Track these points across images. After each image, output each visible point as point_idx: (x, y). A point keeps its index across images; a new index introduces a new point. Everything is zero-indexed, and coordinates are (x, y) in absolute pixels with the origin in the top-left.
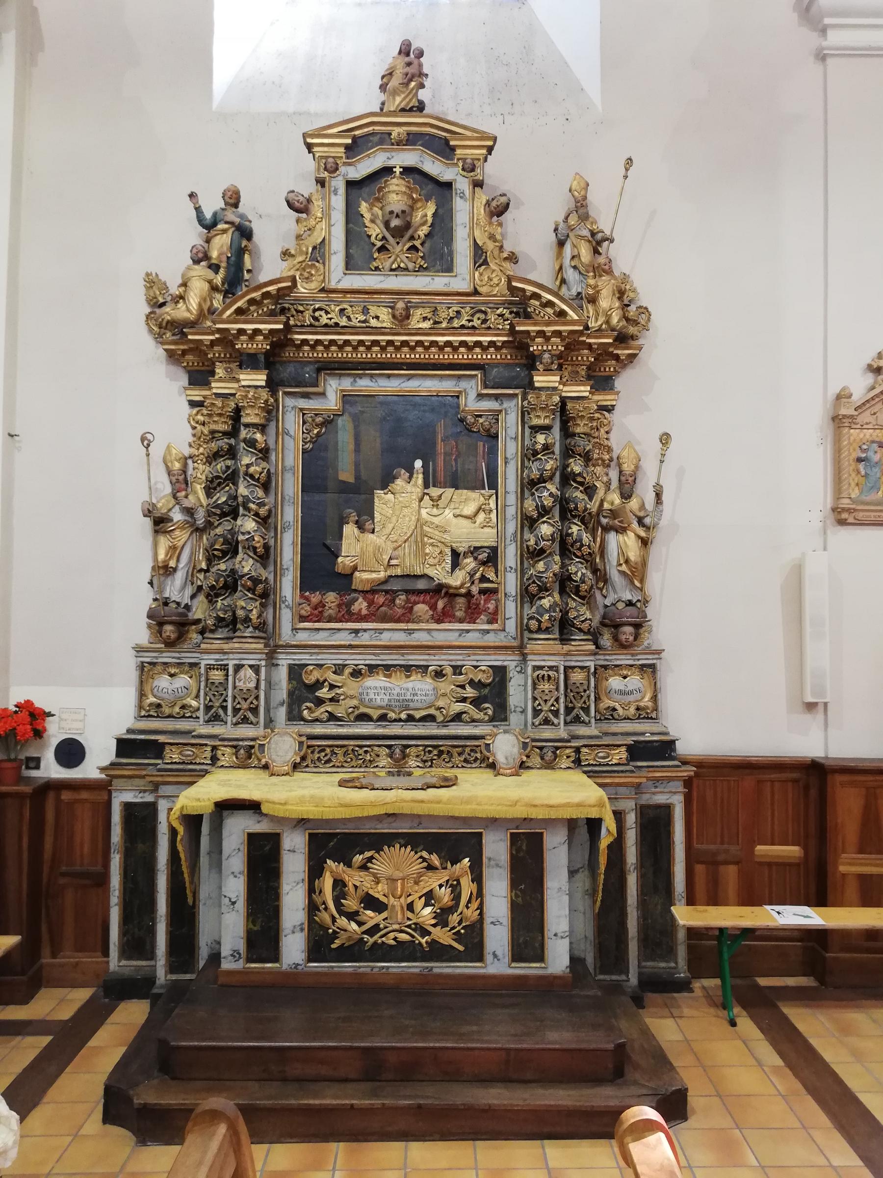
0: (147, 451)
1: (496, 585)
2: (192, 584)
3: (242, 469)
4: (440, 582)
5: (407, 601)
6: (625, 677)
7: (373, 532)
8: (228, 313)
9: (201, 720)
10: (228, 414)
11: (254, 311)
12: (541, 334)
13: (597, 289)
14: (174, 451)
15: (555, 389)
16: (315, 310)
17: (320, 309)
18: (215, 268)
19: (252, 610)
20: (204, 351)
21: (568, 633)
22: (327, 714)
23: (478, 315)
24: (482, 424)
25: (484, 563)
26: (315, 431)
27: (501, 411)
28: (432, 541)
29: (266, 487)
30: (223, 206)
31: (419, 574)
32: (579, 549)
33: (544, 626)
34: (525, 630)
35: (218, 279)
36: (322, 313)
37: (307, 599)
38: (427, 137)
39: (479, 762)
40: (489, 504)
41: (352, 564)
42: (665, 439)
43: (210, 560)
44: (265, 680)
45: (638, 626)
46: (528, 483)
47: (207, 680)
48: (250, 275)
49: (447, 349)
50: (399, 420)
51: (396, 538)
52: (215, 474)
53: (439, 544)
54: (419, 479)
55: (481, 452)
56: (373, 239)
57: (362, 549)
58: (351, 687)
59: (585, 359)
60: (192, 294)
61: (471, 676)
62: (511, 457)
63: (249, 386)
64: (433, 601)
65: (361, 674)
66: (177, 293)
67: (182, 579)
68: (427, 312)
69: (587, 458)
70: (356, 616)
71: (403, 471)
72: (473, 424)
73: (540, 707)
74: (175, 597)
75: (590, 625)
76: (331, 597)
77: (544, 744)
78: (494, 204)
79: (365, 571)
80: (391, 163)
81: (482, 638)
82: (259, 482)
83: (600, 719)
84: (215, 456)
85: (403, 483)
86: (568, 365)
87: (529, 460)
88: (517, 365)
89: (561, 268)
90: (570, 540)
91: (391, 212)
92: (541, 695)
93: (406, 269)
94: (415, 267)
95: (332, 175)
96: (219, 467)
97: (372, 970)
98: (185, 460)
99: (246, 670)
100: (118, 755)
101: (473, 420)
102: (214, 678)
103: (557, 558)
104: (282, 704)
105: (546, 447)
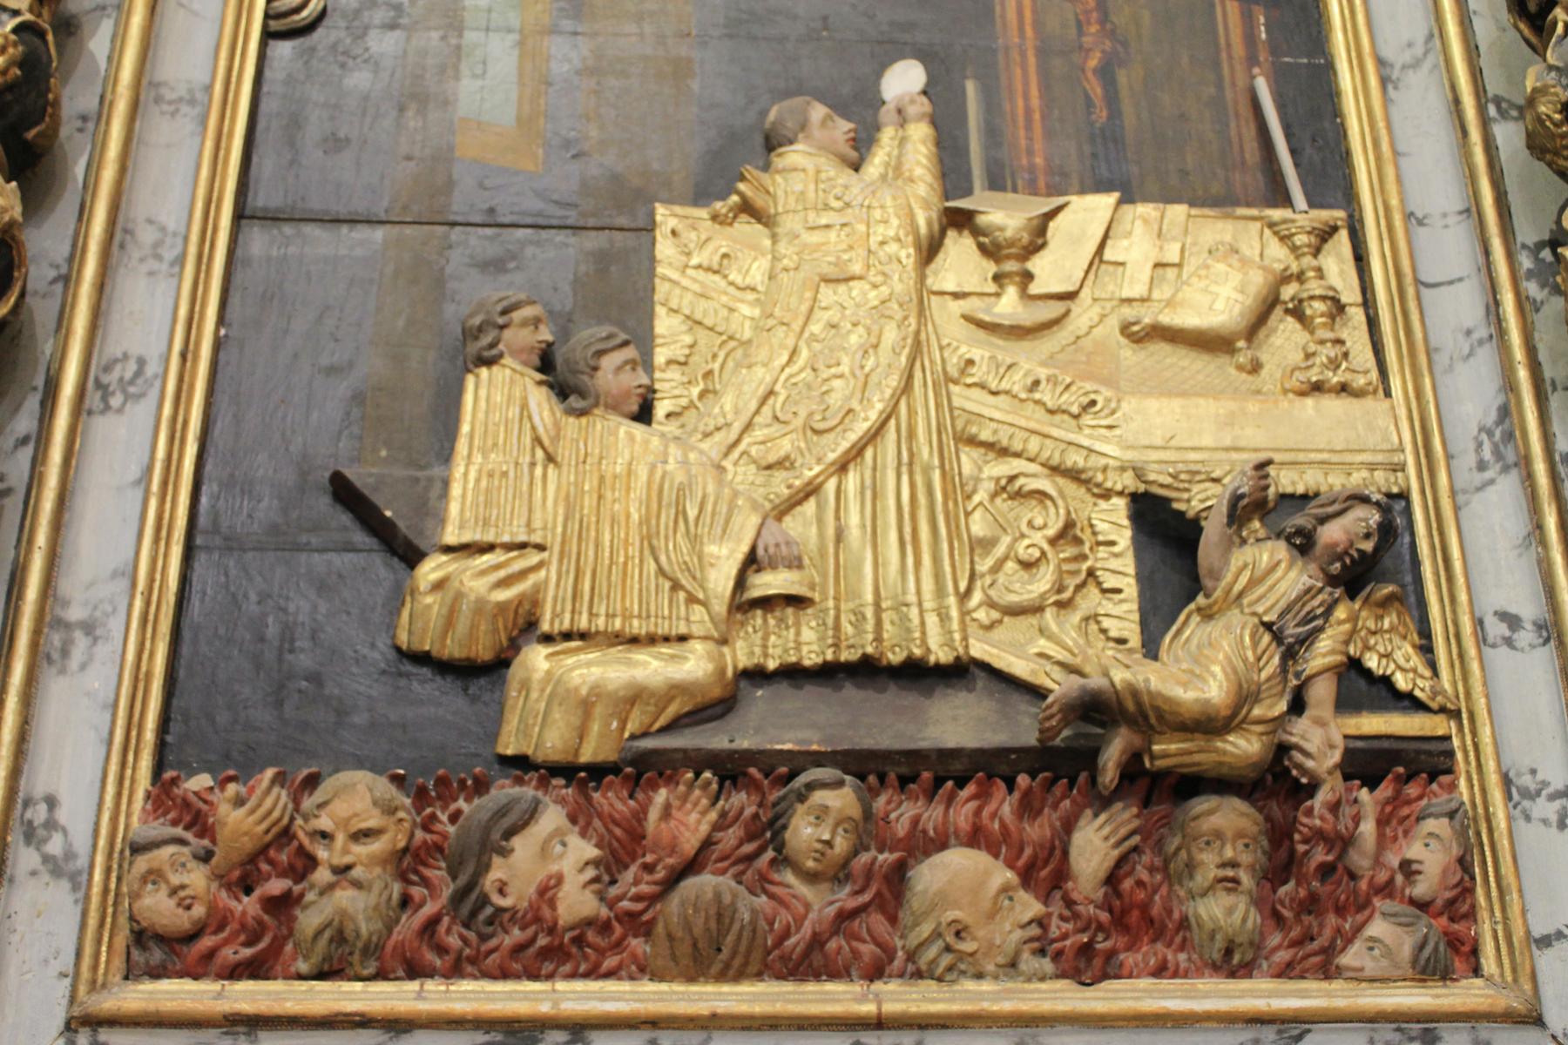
4: (1096, 682)
5: (868, 829)
7: (644, 414)
31: (941, 655)
37: (197, 819)
57: (570, 506)
62: (1407, 57)
64: (1037, 831)
70: (516, 936)
71: (818, 111)
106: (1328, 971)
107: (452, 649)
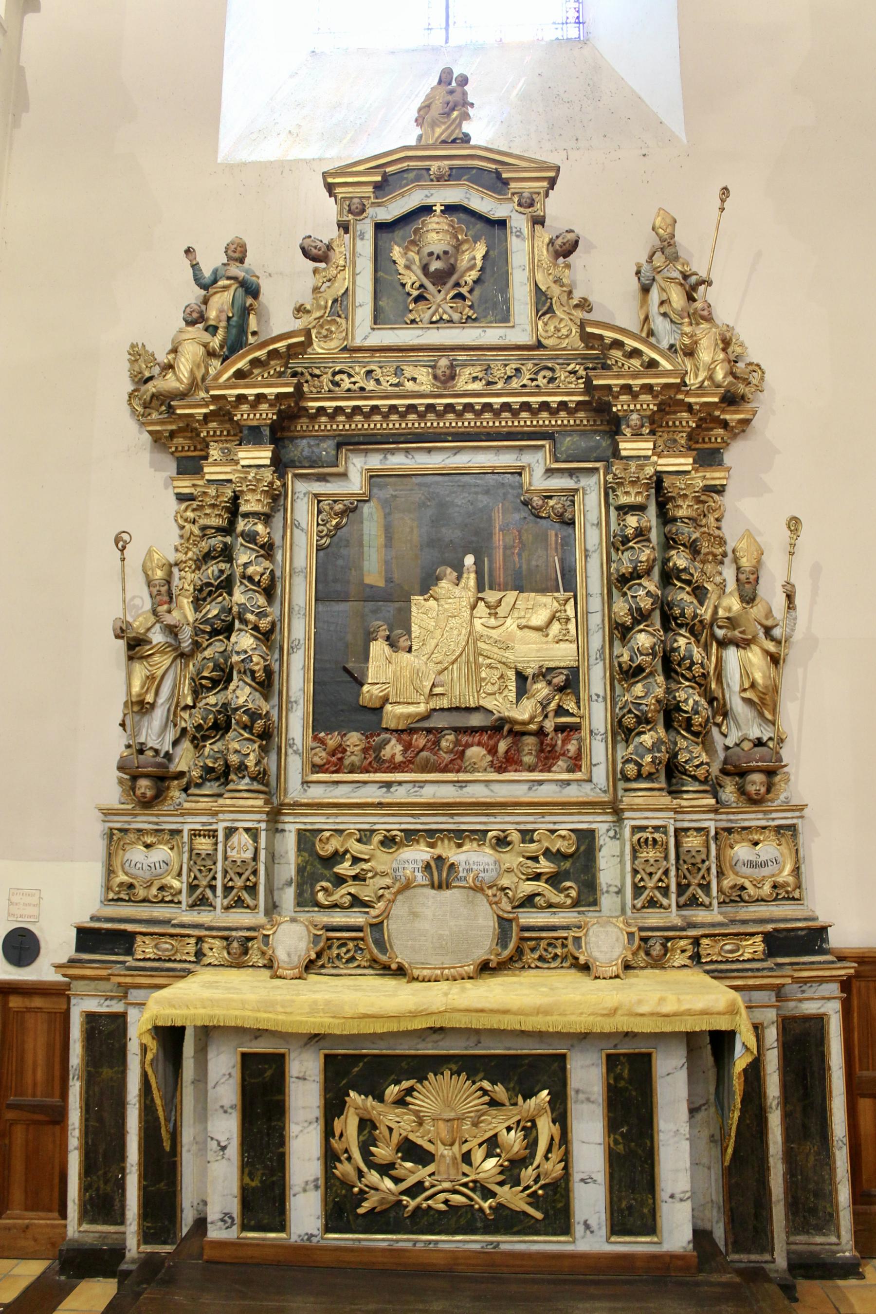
0: (123, 554)
1: (578, 720)
2: (175, 725)
3: (238, 571)
4: (501, 715)
5: (457, 743)
6: (756, 844)
7: (410, 650)
8: (226, 376)
9: (184, 904)
10: (223, 505)
11: (258, 375)
12: (627, 389)
13: (695, 338)
14: (156, 556)
15: (647, 458)
16: (334, 374)
17: (341, 372)
18: (212, 330)
19: (248, 754)
20: (196, 429)
21: (677, 784)
22: (349, 897)
23: (543, 373)
24: (552, 507)
25: (561, 689)
26: (334, 522)
27: (577, 490)
28: (489, 661)
29: (269, 592)
30: (225, 261)
31: (473, 705)
32: (689, 669)
33: (646, 770)
34: (620, 780)
35: (215, 342)
36: (344, 377)
37: (322, 742)
38: (474, 171)
39: (559, 960)
40: (565, 611)
41: (381, 694)
42: (794, 524)
43: (197, 692)
44: (266, 849)
45: (770, 773)
46: (617, 579)
47: (191, 850)
48: (256, 338)
49: (505, 415)
50: (443, 506)
51: (440, 658)
52: (205, 581)
53: (499, 666)
54: (471, 579)
55: (553, 542)
56: (408, 288)
57: (394, 673)
58: (382, 860)
59: (684, 423)
60: (183, 360)
61: (546, 844)
62: (593, 549)
63: (250, 466)
64: (491, 742)
65: (396, 843)
66: (166, 361)
67: (161, 719)
68: (477, 371)
69: (694, 549)
70: (387, 765)
71: (449, 570)
72: (541, 507)
73: (642, 884)
74: (152, 742)
75: (707, 771)
76: (354, 739)
77: (650, 934)
78: (559, 242)
79: (399, 703)
80: (429, 201)
81: (560, 792)
82: (259, 586)
83: (724, 902)
84: (207, 557)
85: (449, 586)
86: (663, 432)
87: (618, 549)
88: (596, 432)
89: (647, 318)
90: (676, 657)
91: (431, 254)
92: (643, 866)
93: (451, 321)
94: (462, 318)
95: (358, 218)
96: (210, 571)
97: (414, 1245)
98: (170, 567)
99: (240, 834)
100: (80, 948)
101: (540, 502)
102: (200, 847)
103: (660, 679)
104: (289, 884)
105: (641, 533)
106: (549, 771)
107: (370, 705)
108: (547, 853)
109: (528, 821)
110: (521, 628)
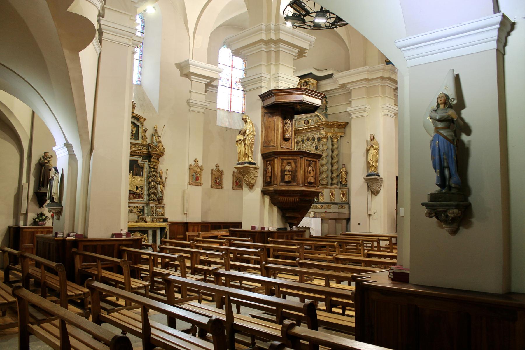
108: (139, 209)
109: (137, 205)
110: (137, 181)
